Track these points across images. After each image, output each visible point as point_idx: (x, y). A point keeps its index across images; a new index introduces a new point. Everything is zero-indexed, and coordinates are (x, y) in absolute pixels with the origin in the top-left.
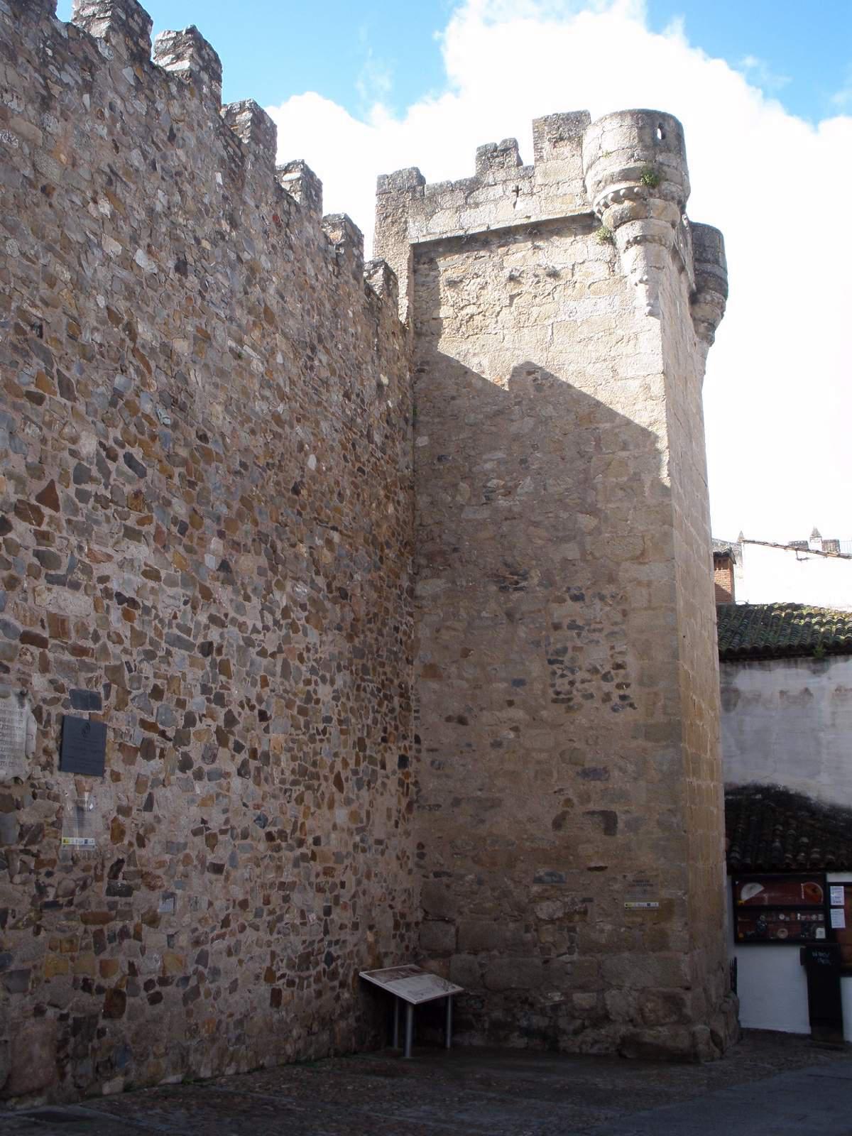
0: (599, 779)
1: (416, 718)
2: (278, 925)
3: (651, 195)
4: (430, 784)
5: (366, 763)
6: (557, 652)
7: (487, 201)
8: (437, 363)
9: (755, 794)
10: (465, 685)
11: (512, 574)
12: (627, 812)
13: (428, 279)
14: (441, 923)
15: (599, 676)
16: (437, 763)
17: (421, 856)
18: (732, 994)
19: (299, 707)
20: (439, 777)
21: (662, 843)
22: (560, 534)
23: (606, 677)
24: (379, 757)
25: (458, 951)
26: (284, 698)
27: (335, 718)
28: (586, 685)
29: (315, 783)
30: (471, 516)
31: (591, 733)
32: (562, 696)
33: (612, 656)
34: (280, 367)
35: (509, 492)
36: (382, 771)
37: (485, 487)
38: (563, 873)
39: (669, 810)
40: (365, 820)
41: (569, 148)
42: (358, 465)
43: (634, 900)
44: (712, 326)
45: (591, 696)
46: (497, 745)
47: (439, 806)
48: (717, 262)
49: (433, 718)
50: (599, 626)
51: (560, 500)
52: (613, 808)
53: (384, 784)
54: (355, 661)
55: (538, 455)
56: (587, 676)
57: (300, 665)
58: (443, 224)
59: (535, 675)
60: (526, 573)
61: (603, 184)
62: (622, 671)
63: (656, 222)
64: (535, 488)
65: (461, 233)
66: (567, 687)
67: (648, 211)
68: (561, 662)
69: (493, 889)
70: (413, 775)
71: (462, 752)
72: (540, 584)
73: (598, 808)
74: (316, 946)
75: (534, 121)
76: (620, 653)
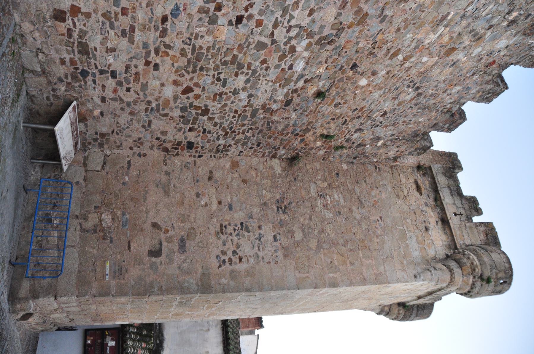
0: (179, 248)
1: (211, 156)
2: (108, 24)
3: (474, 277)
4: (177, 161)
5: (195, 115)
6: (247, 227)
7: (454, 200)
8: (380, 175)
9: (159, 340)
10: (229, 180)
11: (285, 206)
12: (161, 263)
13: (416, 173)
14: (102, 163)
15: (235, 249)
16: (189, 165)
17: (139, 155)
18: (56, 328)
19: (238, 55)
20: (181, 165)
21: (143, 283)
22: (306, 230)
23: (234, 252)
24: (196, 126)
25: (86, 171)
26: (245, 43)
27: (224, 90)
28: (230, 242)
29: (190, 69)
30: (312, 187)
31: (205, 244)
32: (224, 229)
33: (246, 256)
34: (419, 60)
35: (325, 206)
36: (188, 129)
37: (326, 194)
38: (127, 227)
39: (162, 287)
40: (164, 112)
41: (484, 238)
42: (348, 119)
43: (110, 266)
44: (387, 314)
45: (224, 245)
46: (198, 195)
47: (166, 165)
48: (417, 316)
49: (212, 164)
50: (261, 249)
51: (323, 231)
52: (164, 256)
53: (180, 130)
54: (251, 109)
55: (344, 220)
56: (235, 243)
57: (260, 60)
58: (442, 180)
59: (235, 215)
60: (286, 213)
61: (476, 253)
62: (238, 261)
63: (461, 280)
64: (328, 219)
65: (439, 188)
66: (229, 232)
67: (466, 275)
68: (242, 229)
69: (120, 190)
70: (182, 153)
71: (194, 177)
72: (281, 220)
73: (163, 247)
74: (93, 61)
75: (492, 223)
76: (248, 260)
